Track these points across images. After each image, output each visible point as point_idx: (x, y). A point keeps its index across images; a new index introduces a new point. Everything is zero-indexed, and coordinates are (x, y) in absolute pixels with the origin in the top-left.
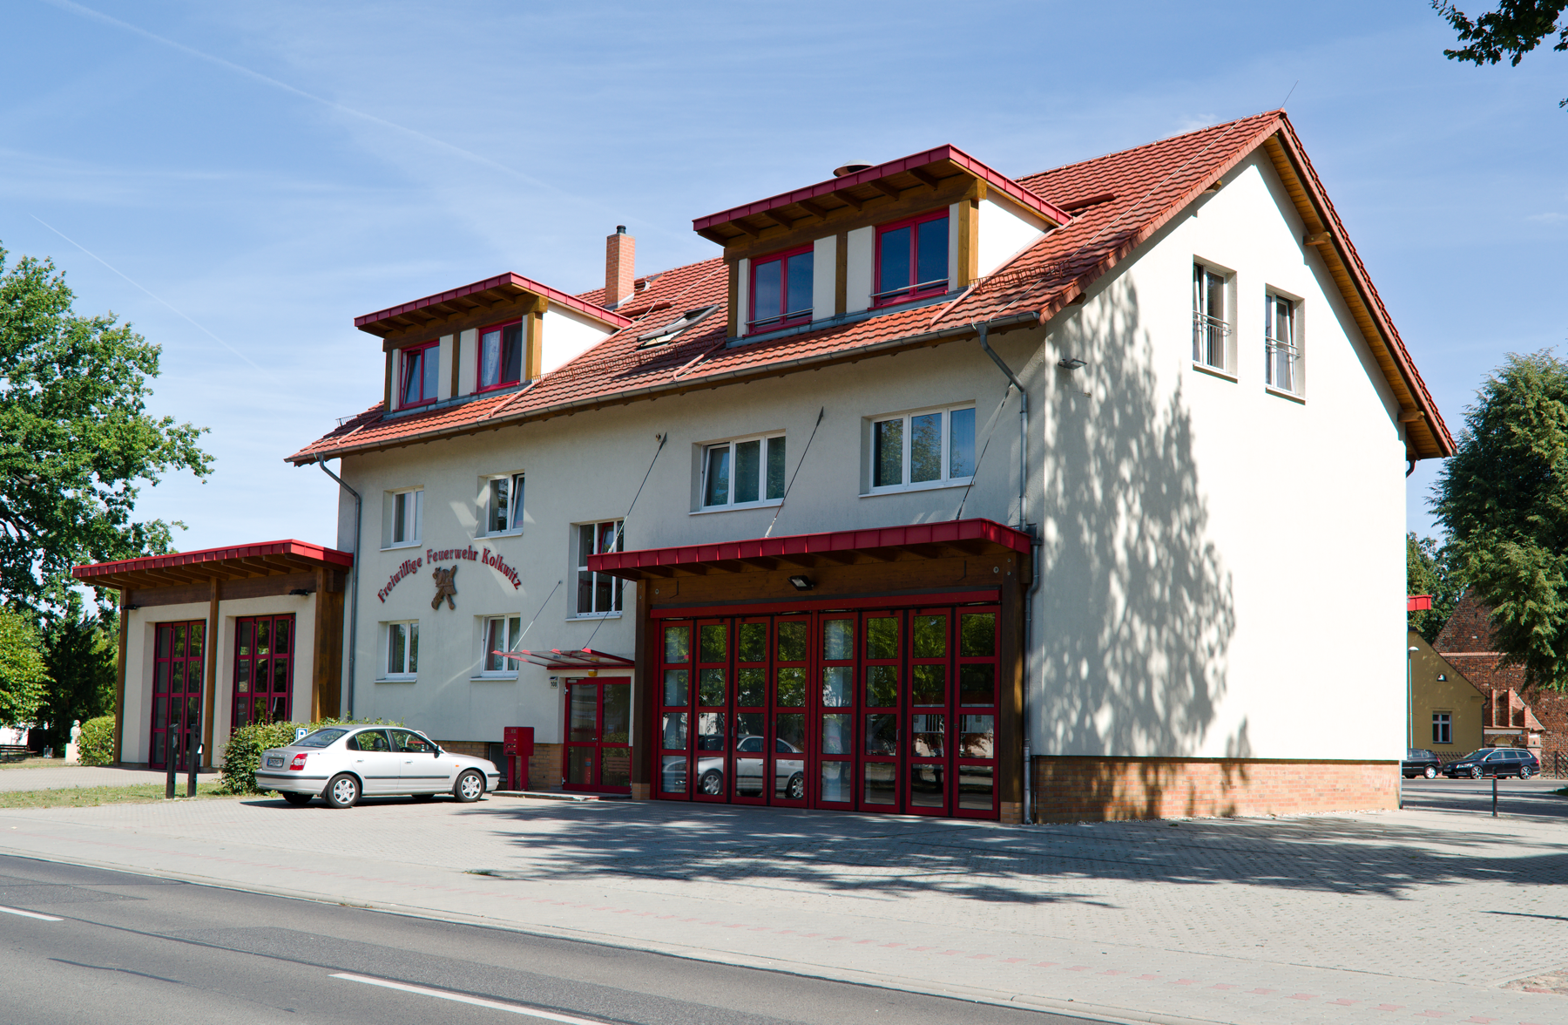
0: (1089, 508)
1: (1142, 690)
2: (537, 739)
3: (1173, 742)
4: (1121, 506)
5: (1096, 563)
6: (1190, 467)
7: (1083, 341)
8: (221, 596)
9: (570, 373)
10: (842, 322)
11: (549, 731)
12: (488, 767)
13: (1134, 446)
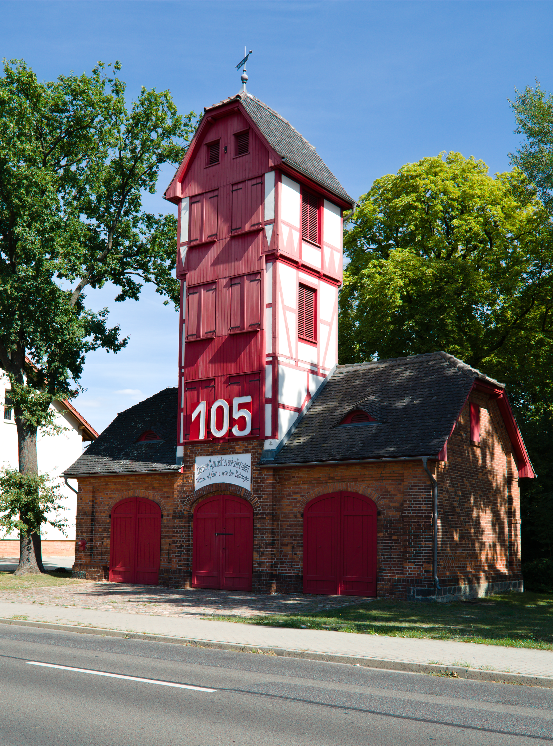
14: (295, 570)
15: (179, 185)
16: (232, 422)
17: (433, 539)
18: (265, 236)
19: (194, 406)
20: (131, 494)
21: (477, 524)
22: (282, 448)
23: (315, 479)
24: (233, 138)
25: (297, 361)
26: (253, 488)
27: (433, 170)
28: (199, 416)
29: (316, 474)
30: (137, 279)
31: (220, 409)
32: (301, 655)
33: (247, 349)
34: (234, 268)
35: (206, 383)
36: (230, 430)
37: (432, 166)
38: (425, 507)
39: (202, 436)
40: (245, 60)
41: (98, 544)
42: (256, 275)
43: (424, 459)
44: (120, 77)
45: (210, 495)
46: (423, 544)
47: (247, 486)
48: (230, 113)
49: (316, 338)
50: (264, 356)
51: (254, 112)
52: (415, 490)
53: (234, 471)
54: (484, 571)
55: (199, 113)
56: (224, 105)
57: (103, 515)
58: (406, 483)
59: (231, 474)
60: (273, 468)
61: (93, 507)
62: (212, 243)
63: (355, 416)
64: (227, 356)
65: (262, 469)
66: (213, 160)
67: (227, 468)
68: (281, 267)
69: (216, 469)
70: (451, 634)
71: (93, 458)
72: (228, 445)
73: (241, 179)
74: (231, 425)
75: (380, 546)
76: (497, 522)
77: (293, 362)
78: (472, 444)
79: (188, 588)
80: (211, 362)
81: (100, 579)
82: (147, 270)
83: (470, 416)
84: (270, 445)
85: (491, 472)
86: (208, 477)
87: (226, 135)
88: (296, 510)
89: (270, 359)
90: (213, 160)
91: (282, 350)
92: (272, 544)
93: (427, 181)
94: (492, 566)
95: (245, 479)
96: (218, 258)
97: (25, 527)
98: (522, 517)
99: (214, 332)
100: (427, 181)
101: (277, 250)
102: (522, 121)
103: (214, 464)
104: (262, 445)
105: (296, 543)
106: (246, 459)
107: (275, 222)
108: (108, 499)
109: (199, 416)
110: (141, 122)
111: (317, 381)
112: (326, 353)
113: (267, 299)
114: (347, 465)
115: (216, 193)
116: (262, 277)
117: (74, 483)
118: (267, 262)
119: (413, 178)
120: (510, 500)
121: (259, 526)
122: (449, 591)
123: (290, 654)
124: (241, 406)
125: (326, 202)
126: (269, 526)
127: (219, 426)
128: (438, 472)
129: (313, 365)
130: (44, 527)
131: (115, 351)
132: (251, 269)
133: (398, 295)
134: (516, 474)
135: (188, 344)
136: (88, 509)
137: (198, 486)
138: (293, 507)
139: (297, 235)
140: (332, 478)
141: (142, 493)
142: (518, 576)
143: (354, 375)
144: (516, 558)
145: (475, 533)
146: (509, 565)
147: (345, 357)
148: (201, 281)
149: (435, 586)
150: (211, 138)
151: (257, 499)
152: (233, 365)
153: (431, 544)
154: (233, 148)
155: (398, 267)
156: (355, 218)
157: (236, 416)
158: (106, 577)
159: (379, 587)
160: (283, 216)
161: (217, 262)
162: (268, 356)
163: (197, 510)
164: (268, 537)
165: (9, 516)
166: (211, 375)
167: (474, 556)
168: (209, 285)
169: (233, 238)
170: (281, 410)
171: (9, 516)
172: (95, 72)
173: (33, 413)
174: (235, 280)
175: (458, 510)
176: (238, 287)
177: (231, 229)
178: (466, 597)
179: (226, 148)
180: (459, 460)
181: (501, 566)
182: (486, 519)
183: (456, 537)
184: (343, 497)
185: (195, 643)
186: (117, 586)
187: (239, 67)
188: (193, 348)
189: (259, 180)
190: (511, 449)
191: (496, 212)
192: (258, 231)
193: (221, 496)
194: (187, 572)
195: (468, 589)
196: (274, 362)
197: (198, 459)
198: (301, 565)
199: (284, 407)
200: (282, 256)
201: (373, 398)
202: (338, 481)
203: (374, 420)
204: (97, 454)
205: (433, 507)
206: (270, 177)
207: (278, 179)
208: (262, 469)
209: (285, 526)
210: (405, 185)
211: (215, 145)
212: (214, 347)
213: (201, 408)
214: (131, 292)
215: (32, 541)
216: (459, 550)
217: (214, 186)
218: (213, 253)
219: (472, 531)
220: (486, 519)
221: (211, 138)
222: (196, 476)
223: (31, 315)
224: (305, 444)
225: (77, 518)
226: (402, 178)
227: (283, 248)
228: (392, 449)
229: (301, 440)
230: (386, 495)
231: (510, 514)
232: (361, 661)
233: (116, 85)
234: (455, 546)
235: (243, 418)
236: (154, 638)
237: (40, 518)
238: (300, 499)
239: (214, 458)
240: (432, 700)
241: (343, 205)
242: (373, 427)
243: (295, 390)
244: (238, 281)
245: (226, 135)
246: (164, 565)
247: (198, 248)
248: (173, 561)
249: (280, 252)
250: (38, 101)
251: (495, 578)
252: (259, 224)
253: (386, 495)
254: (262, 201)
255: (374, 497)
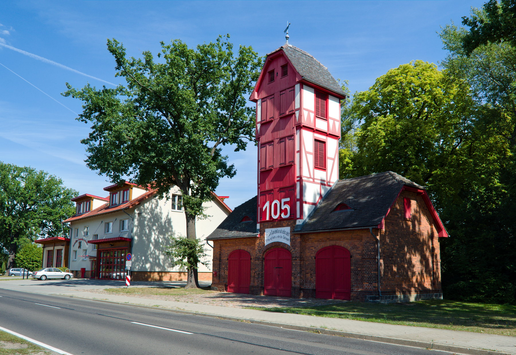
0: (145, 234)
1: (157, 261)
2: (86, 270)
3: (165, 269)
4: (153, 233)
5: (147, 242)
6: (171, 227)
7: (145, 209)
8: (54, 246)
9: (101, 209)
10: (119, 205)
11: (88, 268)
12: (71, 274)
13: (157, 224)
14: (311, 286)
15: (256, 93)
16: (281, 211)
17: (377, 269)
18: (295, 117)
19: (264, 203)
20: (237, 248)
21: (410, 262)
22: (305, 224)
23: (321, 239)
24: (280, 68)
25: (314, 179)
26: (291, 244)
27: (405, 71)
28: (266, 209)
29: (321, 237)
30: (244, 140)
31: (276, 205)
32: (260, 322)
33: (288, 174)
34: (282, 133)
35: (270, 192)
36: (280, 215)
37: (404, 69)
38: (373, 253)
39: (268, 219)
40: (288, 28)
41: (223, 273)
42: (291, 137)
43: (371, 228)
44: (230, 41)
45: (272, 248)
46: (372, 272)
47: (288, 243)
48: (278, 55)
49: (325, 167)
50: (296, 177)
51: (290, 54)
52: (368, 244)
53: (281, 236)
54: (415, 288)
55: (265, 55)
56: (277, 52)
57: (225, 258)
58: (363, 241)
59: (281, 237)
60: (301, 234)
61: (220, 254)
62: (271, 121)
63: (341, 206)
64: (279, 178)
65: (295, 234)
66: (272, 80)
67: (279, 234)
68: (304, 132)
69: (275, 235)
70: (367, 317)
71: (221, 230)
72: (279, 223)
73: (284, 88)
74: (281, 213)
75: (352, 274)
76: (424, 260)
77: (312, 180)
78: (405, 219)
79: (262, 295)
80: (272, 181)
81: (223, 291)
82: (251, 135)
83: (404, 205)
84: (299, 222)
85: (420, 234)
86: (271, 239)
87: (277, 67)
88: (312, 255)
89: (299, 179)
90: (272, 80)
91: (305, 173)
92: (301, 273)
93: (402, 78)
94: (421, 284)
95: (287, 240)
96: (274, 129)
97: (190, 265)
98: (441, 258)
99: (273, 166)
100: (402, 78)
101: (301, 123)
102: (446, 43)
103: (273, 233)
104: (295, 223)
105: (312, 272)
106: (288, 229)
107: (300, 109)
108: (227, 251)
109: (266, 209)
110: (241, 63)
111: (325, 189)
112: (332, 175)
113: (297, 149)
114: (335, 232)
115: (273, 96)
116: (295, 137)
117: (211, 243)
118: (297, 130)
119: (393, 76)
120: (433, 249)
121: (294, 263)
122: (389, 298)
123: (256, 322)
124: (285, 203)
125: (330, 96)
126: (299, 264)
127: (275, 213)
128: (381, 235)
129: (322, 180)
130: (199, 265)
131: (231, 177)
132: (289, 134)
133: (383, 140)
134: (436, 234)
135: (261, 172)
136: (218, 256)
137: (266, 243)
138: (310, 254)
139: (312, 115)
140: (328, 239)
141: (242, 247)
142: (439, 291)
143: (344, 186)
144: (438, 281)
145: (408, 267)
146: (433, 283)
147: (342, 174)
148: (267, 141)
149: (379, 295)
150: (270, 69)
151: (293, 250)
152: (282, 182)
153: (376, 273)
154: (280, 73)
155: (383, 124)
156: (365, 100)
157: (283, 208)
158: (226, 290)
159: (351, 295)
160: (305, 105)
161: (274, 131)
162: (298, 177)
163: (266, 256)
164: (298, 269)
165: (182, 260)
166: (271, 188)
167: (408, 280)
168: (270, 143)
169: (281, 118)
170: (304, 205)
171: (182, 260)
172: (218, 40)
173: (192, 209)
174: (282, 140)
175: (396, 255)
176: (283, 143)
177: (280, 114)
178: (401, 301)
179: (277, 73)
180: (397, 228)
181: (427, 284)
182: (416, 260)
183: (395, 269)
184: (334, 248)
185: (221, 317)
186: (229, 294)
187: (285, 31)
188: (264, 174)
189: (292, 89)
190: (433, 221)
191: (439, 92)
192: (292, 114)
193: (277, 248)
194: (262, 287)
195: (402, 297)
196: (301, 180)
197: (266, 230)
198: (315, 284)
199: (306, 203)
200: (304, 126)
201: (350, 198)
202: (331, 240)
203: (350, 208)
204: (223, 228)
205: (377, 253)
206: (297, 87)
207: (301, 87)
208: (295, 234)
209: (307, 264)
210: (389, 81)
211: (272, 72)
212: (273, 173)
213: (267, 204)
214: (242, 146)
215: (194, 272)
216: (397, 276)
217: (272, 93)
218: (272, 126)
219: (406, 266)
220: (416, 260)
221: (270, 69)
222: (266, 239)
223: (189, 161)
224: (316, 221)
225: (213, 260)
226: (389, 77)
227: (305, 121)
228: (356, 223)
229: (315, 220)
230: (355, 247)
231: (433, 255)
232: (283, 325)
233: (228, 45)
234: (394, 274)
235: (286, 209)
236: (205, 315)
237: (196, 261)
238: (314, 249)
239: (274, 229)
240: (291, 341)
241: (340, 97)
242: (349, 212)
243: (312, 193)
244: (283, 140)
245: (277, 67)
246: (252, 284)
247: (265, 124)
248: (255, 282)
249: (302, 124)
250: (188, 58)
251: (422, 291)
252: (293, 111)
253: (355, 247)
254: (294, 99)
255: (349, 248)
